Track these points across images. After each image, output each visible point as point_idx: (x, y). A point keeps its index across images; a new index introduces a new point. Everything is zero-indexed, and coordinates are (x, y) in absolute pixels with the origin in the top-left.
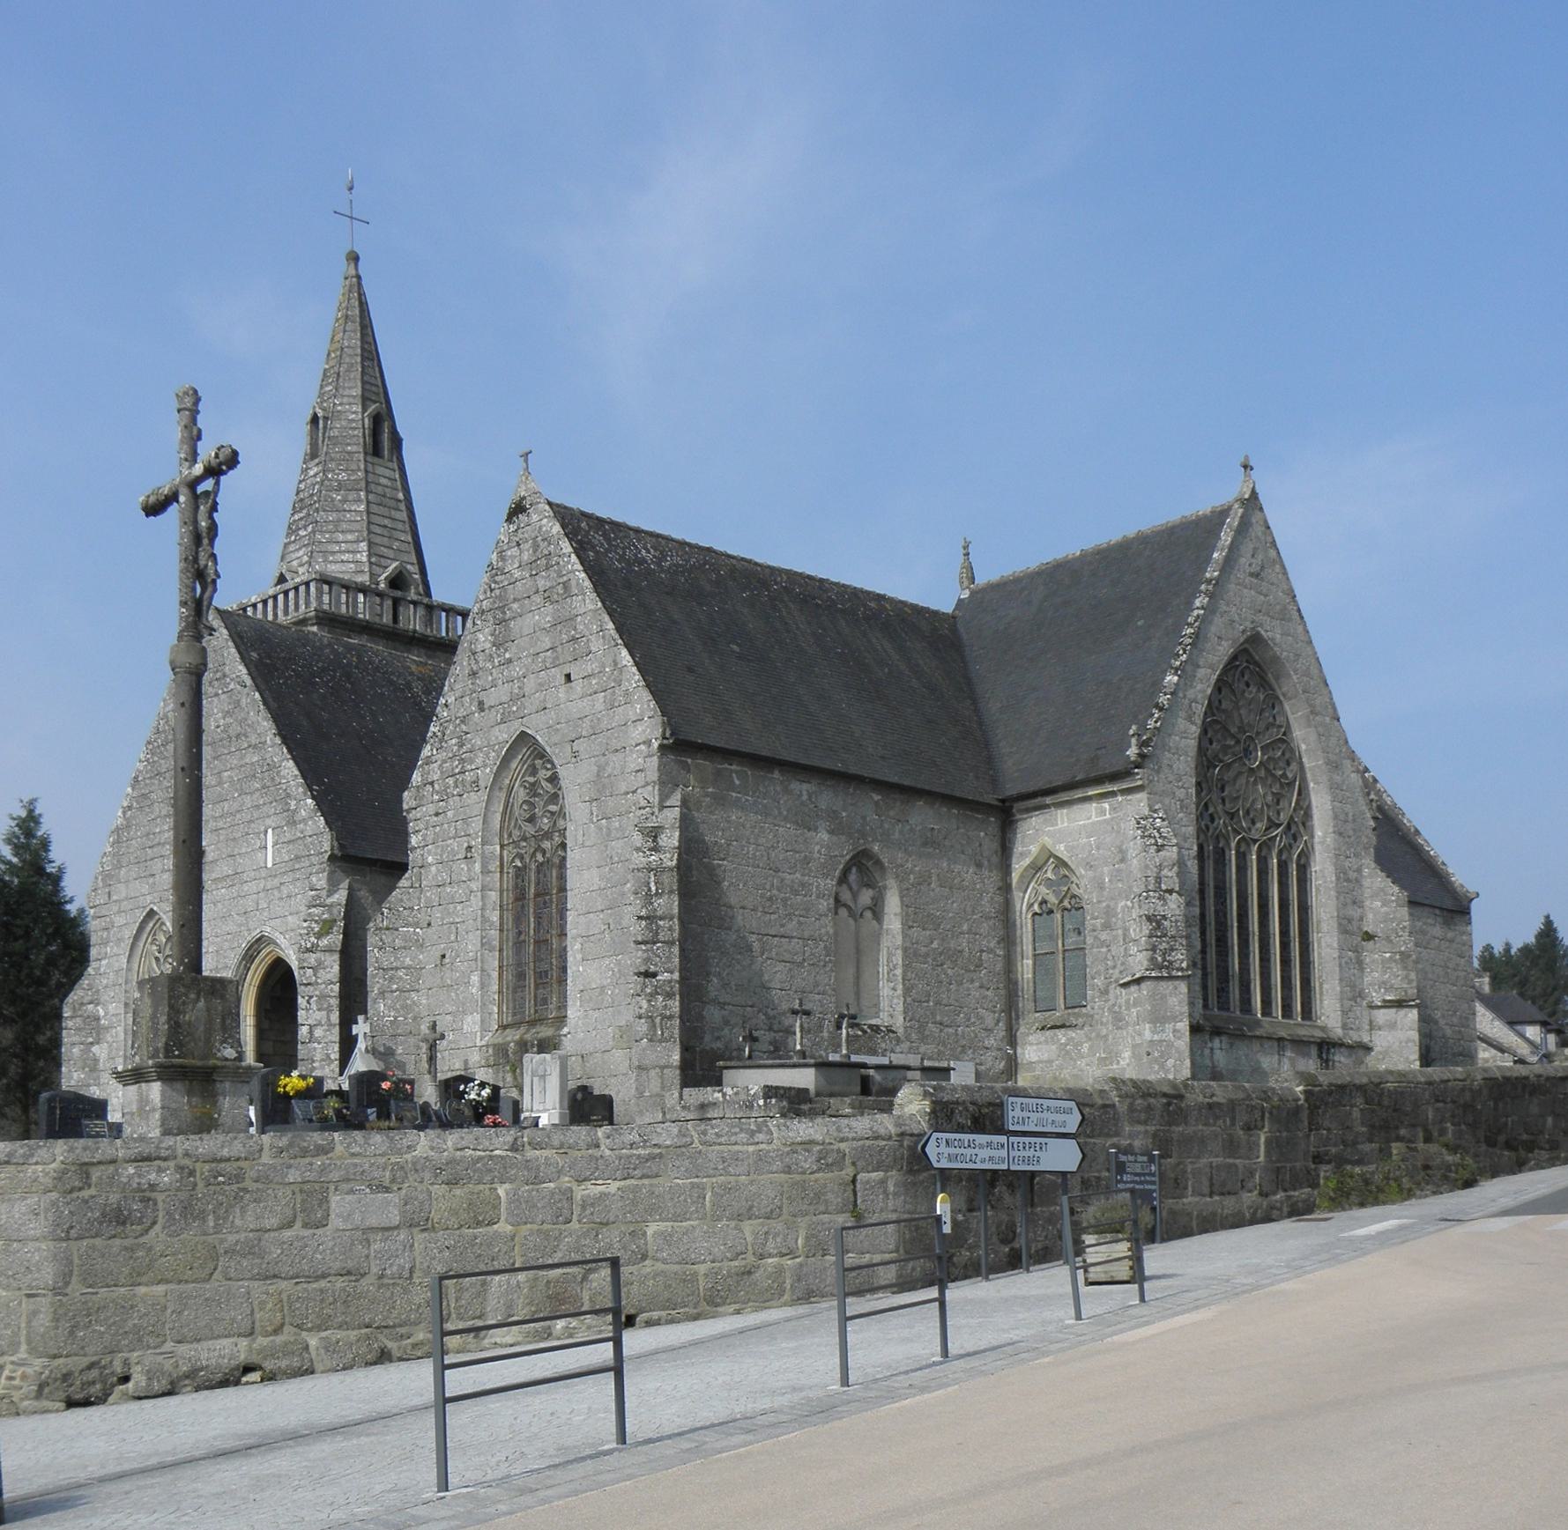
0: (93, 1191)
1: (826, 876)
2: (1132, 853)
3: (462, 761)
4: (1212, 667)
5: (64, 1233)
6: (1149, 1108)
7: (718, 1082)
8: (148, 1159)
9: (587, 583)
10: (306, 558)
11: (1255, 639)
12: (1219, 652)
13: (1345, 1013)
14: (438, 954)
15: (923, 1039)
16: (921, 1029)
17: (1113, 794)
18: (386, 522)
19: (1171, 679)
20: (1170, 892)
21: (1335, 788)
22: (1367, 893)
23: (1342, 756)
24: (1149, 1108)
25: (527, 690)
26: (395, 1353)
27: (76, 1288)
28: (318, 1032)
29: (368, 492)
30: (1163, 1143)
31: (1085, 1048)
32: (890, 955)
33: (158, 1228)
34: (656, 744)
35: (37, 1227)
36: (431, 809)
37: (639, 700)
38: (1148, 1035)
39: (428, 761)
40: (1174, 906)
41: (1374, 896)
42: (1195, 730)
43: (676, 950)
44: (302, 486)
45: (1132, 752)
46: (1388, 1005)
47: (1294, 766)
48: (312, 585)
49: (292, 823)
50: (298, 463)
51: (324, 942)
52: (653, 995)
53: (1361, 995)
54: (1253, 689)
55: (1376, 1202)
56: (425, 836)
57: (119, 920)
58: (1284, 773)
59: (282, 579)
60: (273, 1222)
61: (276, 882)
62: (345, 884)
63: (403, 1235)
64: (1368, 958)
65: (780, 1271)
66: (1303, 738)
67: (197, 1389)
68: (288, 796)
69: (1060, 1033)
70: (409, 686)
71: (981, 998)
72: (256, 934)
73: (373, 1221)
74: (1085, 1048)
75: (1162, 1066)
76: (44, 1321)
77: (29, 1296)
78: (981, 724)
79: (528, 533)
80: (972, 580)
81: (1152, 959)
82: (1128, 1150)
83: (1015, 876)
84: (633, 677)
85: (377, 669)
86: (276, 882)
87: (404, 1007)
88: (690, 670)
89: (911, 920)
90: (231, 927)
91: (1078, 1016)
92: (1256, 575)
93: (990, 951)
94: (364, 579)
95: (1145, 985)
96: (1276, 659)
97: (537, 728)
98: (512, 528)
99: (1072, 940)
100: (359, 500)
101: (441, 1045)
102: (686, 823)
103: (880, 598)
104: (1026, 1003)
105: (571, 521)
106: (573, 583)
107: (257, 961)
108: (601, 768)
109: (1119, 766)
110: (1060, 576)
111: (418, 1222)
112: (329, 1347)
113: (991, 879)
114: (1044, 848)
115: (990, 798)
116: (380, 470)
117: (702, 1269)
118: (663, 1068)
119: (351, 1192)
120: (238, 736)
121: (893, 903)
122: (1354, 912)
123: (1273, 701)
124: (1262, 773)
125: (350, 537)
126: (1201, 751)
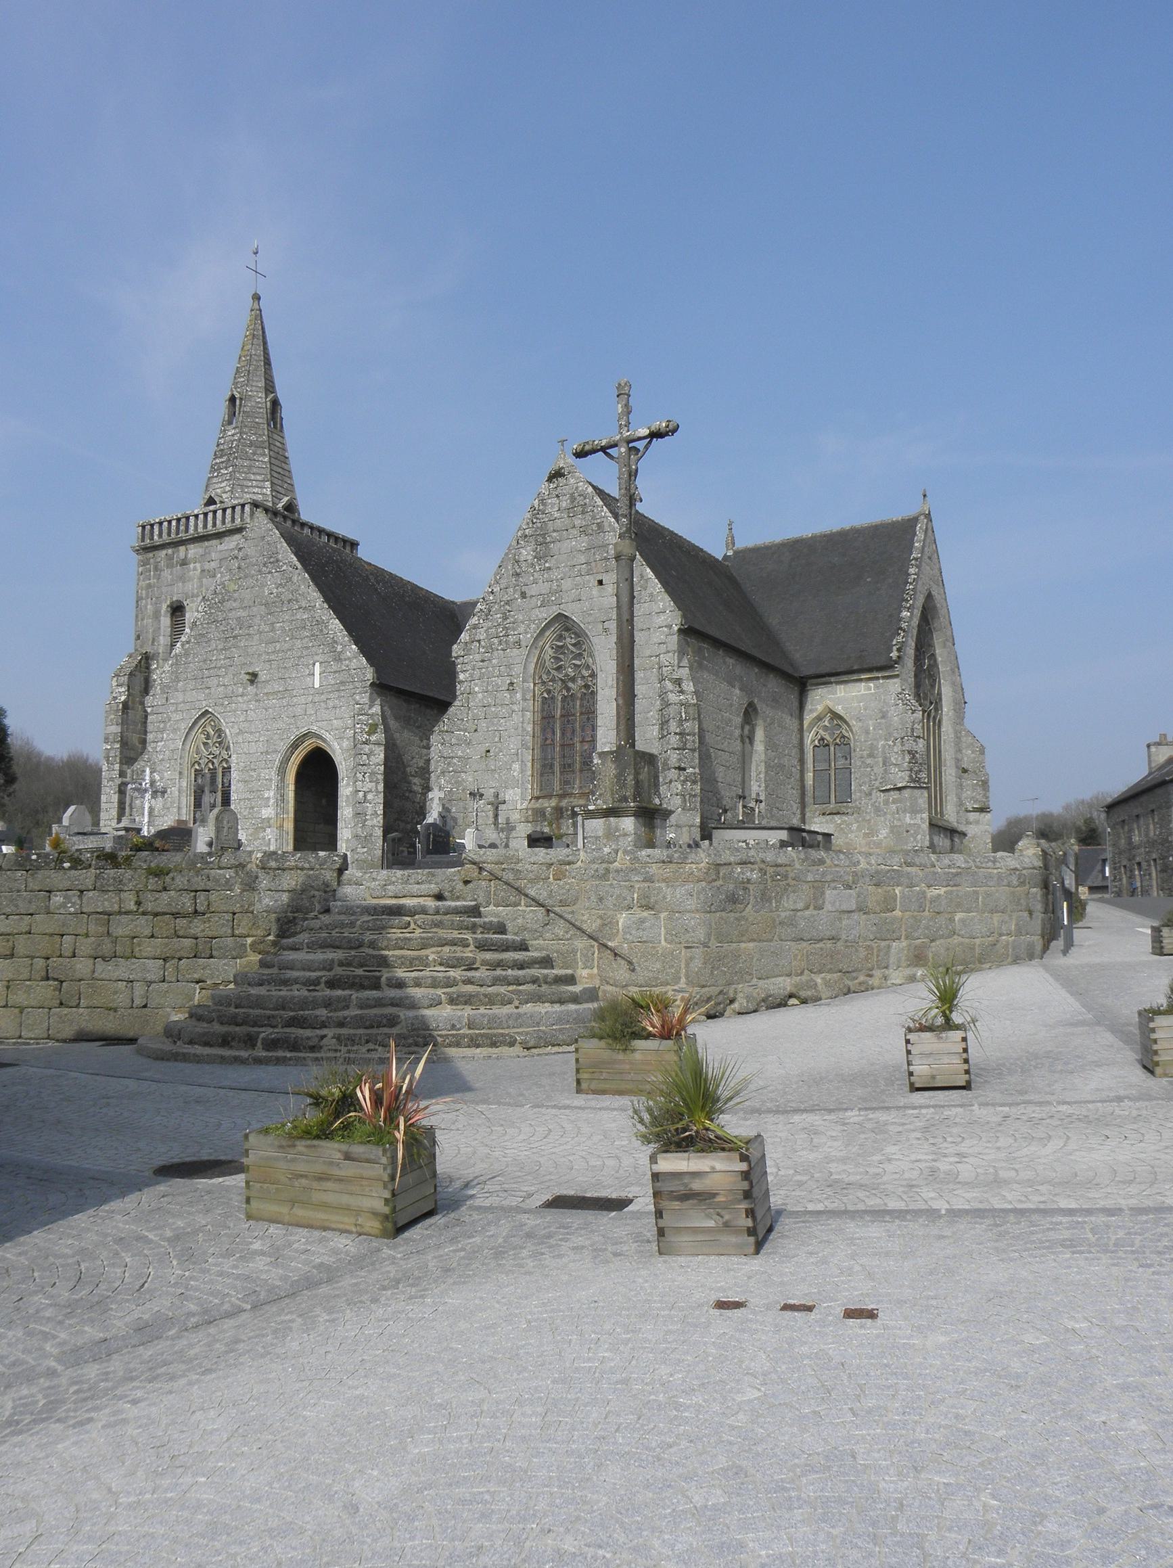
0: (721, 882)
3: (505, 628)
8: (745, 863)
10: (228, 489)
14: (484, 750)
17: (878, 678)
25: (564, 588)
26: (852, 989)
27: (713, 943)
28: (370, 797)
29: (270, 450)
31: (855, 827)
32: (758, 765)
33: (750, 906)
34: (676, 628)
35: (691, 904)
36: (478, 657)
37: (662, 600)
38: (908, 820)
41: (967, 747)
43: (696, 754)
45: (894, 654)
46: (975, 810)
48: (247, 508)
49: (338, 659)
51: (373, 738)
52: (684, 782)
56: (471, 675)
59: (211, 501)
60: (800, 905)
63: (855, 916)
67: (767, 1008)
68: (336, 642)
69: (837, 818)
70: (368, 579)
71: (793, 794)
72: (304, 730)
73: (844, 907)
74: (855, 827)
76: (697, 964)
77: (687, 948)
80: (734, 544)
81: (910, 776)
89: (770, 745)
90: (280, 725)
91: (847, 808)
95: (906, 793)
97: (574, 612)
98: (552, 486)
99: (841, 763)
100: (265, 455)
101: (501, 807)
104: (809, 799)
106: (606, 524)
107: (300, 748)
109: (882, 662)
110: (797, 548)
112: (827, 983)
113: (796, 723)
116: (275, 437)
117: (977, 941)
118: (690, 826)
119: (835, 888)
120: (289, 601)
125: (258, 478)
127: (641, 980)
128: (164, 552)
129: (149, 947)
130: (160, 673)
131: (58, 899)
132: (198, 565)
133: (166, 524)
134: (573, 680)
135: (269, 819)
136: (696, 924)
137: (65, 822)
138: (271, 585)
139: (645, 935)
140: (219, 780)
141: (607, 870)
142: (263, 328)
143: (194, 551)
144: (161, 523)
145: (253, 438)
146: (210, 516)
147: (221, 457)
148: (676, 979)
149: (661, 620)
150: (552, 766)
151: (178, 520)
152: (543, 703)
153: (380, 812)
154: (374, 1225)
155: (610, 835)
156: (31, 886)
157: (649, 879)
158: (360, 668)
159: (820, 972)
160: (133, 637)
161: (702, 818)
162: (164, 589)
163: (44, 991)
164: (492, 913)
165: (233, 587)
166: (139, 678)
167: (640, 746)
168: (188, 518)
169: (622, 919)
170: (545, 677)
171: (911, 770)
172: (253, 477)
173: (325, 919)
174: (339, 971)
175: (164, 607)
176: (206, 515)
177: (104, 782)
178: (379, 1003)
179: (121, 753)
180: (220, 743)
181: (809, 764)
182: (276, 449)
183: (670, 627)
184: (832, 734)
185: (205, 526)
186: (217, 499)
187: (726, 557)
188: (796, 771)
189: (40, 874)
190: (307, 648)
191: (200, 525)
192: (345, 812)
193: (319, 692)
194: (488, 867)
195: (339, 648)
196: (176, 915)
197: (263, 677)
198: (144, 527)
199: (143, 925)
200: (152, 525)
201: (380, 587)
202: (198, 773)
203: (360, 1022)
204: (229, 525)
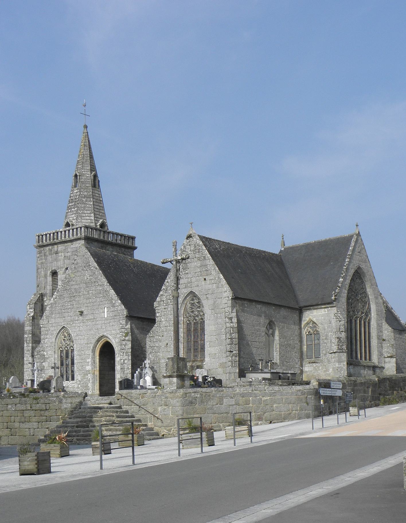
1: (264, 327)
2: (333, 322)
4: (350, 276)
5: (183, 405)
6: (351, 383)
7: (245, 377)
9: (210, 257)
10: (75, 218)
11: (359, 268)
12: (352, 272)
13: (379, 359)
15: (283, 365)
16: (283, 363)
17: (328, 307)
18: (98, 207)
19: (341, 280)
20: (342, 332)
21: (377, 303)
22: (384, 329)
23: (379, 295)
24: (351, 383)
25: (193, 281)
28: (126, 362)
29: (93, 198)
30: (353, 390)
31: (320, 368)
32: (276, 345)
34: (230, 298)
35: (178, 404)
36: (163, 307)
38: (337, 365)
39: (162, 295)
40: (343, 335)
42: (346, 291)
43: (237, 346)
44: (72, 195)
45: (333, 298)
46: (388, 357)
47: (367, 298)
48: (83, 229)
49: (113, 306)
50: (70, 188)
51: (127, 338)
53: (382, 355)
54: (358, 280)
55: (392, 404)
56: (161, 314)
57: (52, 329)
58: (366, 302)
59: (68, 225)
61: (108, 321)
62: (129, 323)
63: (235, 406)
64: (384, 345)
65: (295, 413)
66: (369, 291)
69: (314, 364)
71: (295, 355)
72: (101, 335)
73: (230, 404)
74: (320, 368)
75: (340, 373)
78: (291, 286)
79: (193, 243)
81: (338, 348)
82: (347, 392)
83: (302, 326)
84: (224, 282)
85: (122, 261)
86: (108, 321)
87: (156, 356)
88: (233, 278)
89: (281, 336)
90: (92, 332)
91: (318, 360)
92: (359, 252)
93: (297, 344)
94: (93, 225)
96: (363, 272)
97: (196, 290)
99: (316, 341)
100: (90, 201)
102: (237, 315)
103: (264, 252)
104: (305, 357)
105: (203, 239)
108: (215, 302)
109: (329, 301)
110: (308, 247)
111: (237, 404)
113: (297, 327)
114: (310, 319)
115: (297, 307)
116: (96, 192)
117: (283, 413)
120: (94, 282)
121: (277, 333)
122: (380, 334)
123: (363, 282)
124: (360, 300)
125: (88, 212)
126: (347, 296)
127: (165, 425)
128: (48, 248)
129: (34, 419)
130: (47, 302)
131: (10, 406)
132: (63, 254)
133: (48, 235)
134: (197, 316)
135: (89, 371)
136: (179, 410)
137: (10, 382)
138: (87, 275)
139: (165, 413)
140: (70, 354)
141: (155, 396)
142: (89, 141)
143: (61, 247)
144: (46, 235)
145: (86, 194)
146: (67, 232)
147: (72, 203)
148: (174, 425)
149: (225, 295)
150: (190, 350)
151: (54, 233)
152: (187, 325)
153: (130, 367)
154: (58, 456)
155: (171, 383)
156: (2, 403)
157: (167, 398)
158: (121, 309)
159: (222, 423)
160: (36, 286)
161: (239, 370)
162: (48, 265)
163: (7, 432)
164: (125, 408)
165: (73, 276)
166: (39, 304)
167: (180, 356)
168: (57, 233)
169: (160, 409)
170: (188, 315)
171: (339, 345)
172: (86, 212)
173: (80, 410)
174: (80, 424)
175: (49, 272)
176: (65, 231)
177: (25, 352)
178: (88, 431)
179: (32, 338)
180: (70, 339)
181: (305, 342)
182: (96, 198)
183: (228, 297)
184: (313, 330)
185: (65, 237)
186: (70, 223)
187: (281, 251)
188: (298, 346)
189: (5, 400)
190: (102, 301)
191: (63, 236)
192: (118, 367)
193: (107, 319)
194: (124, 395)
195: (114, 302)
196: (41, 410)
197: (85, 313)
198: (39, 236)
199: (32, 413)
200: (42, 236)
201: (135, 270)
202: (62, 352)
203: (83, 436)
204: (75, 237)
